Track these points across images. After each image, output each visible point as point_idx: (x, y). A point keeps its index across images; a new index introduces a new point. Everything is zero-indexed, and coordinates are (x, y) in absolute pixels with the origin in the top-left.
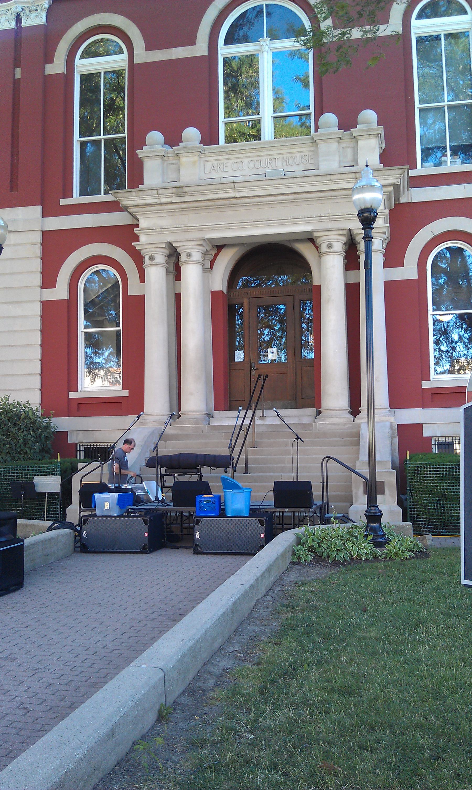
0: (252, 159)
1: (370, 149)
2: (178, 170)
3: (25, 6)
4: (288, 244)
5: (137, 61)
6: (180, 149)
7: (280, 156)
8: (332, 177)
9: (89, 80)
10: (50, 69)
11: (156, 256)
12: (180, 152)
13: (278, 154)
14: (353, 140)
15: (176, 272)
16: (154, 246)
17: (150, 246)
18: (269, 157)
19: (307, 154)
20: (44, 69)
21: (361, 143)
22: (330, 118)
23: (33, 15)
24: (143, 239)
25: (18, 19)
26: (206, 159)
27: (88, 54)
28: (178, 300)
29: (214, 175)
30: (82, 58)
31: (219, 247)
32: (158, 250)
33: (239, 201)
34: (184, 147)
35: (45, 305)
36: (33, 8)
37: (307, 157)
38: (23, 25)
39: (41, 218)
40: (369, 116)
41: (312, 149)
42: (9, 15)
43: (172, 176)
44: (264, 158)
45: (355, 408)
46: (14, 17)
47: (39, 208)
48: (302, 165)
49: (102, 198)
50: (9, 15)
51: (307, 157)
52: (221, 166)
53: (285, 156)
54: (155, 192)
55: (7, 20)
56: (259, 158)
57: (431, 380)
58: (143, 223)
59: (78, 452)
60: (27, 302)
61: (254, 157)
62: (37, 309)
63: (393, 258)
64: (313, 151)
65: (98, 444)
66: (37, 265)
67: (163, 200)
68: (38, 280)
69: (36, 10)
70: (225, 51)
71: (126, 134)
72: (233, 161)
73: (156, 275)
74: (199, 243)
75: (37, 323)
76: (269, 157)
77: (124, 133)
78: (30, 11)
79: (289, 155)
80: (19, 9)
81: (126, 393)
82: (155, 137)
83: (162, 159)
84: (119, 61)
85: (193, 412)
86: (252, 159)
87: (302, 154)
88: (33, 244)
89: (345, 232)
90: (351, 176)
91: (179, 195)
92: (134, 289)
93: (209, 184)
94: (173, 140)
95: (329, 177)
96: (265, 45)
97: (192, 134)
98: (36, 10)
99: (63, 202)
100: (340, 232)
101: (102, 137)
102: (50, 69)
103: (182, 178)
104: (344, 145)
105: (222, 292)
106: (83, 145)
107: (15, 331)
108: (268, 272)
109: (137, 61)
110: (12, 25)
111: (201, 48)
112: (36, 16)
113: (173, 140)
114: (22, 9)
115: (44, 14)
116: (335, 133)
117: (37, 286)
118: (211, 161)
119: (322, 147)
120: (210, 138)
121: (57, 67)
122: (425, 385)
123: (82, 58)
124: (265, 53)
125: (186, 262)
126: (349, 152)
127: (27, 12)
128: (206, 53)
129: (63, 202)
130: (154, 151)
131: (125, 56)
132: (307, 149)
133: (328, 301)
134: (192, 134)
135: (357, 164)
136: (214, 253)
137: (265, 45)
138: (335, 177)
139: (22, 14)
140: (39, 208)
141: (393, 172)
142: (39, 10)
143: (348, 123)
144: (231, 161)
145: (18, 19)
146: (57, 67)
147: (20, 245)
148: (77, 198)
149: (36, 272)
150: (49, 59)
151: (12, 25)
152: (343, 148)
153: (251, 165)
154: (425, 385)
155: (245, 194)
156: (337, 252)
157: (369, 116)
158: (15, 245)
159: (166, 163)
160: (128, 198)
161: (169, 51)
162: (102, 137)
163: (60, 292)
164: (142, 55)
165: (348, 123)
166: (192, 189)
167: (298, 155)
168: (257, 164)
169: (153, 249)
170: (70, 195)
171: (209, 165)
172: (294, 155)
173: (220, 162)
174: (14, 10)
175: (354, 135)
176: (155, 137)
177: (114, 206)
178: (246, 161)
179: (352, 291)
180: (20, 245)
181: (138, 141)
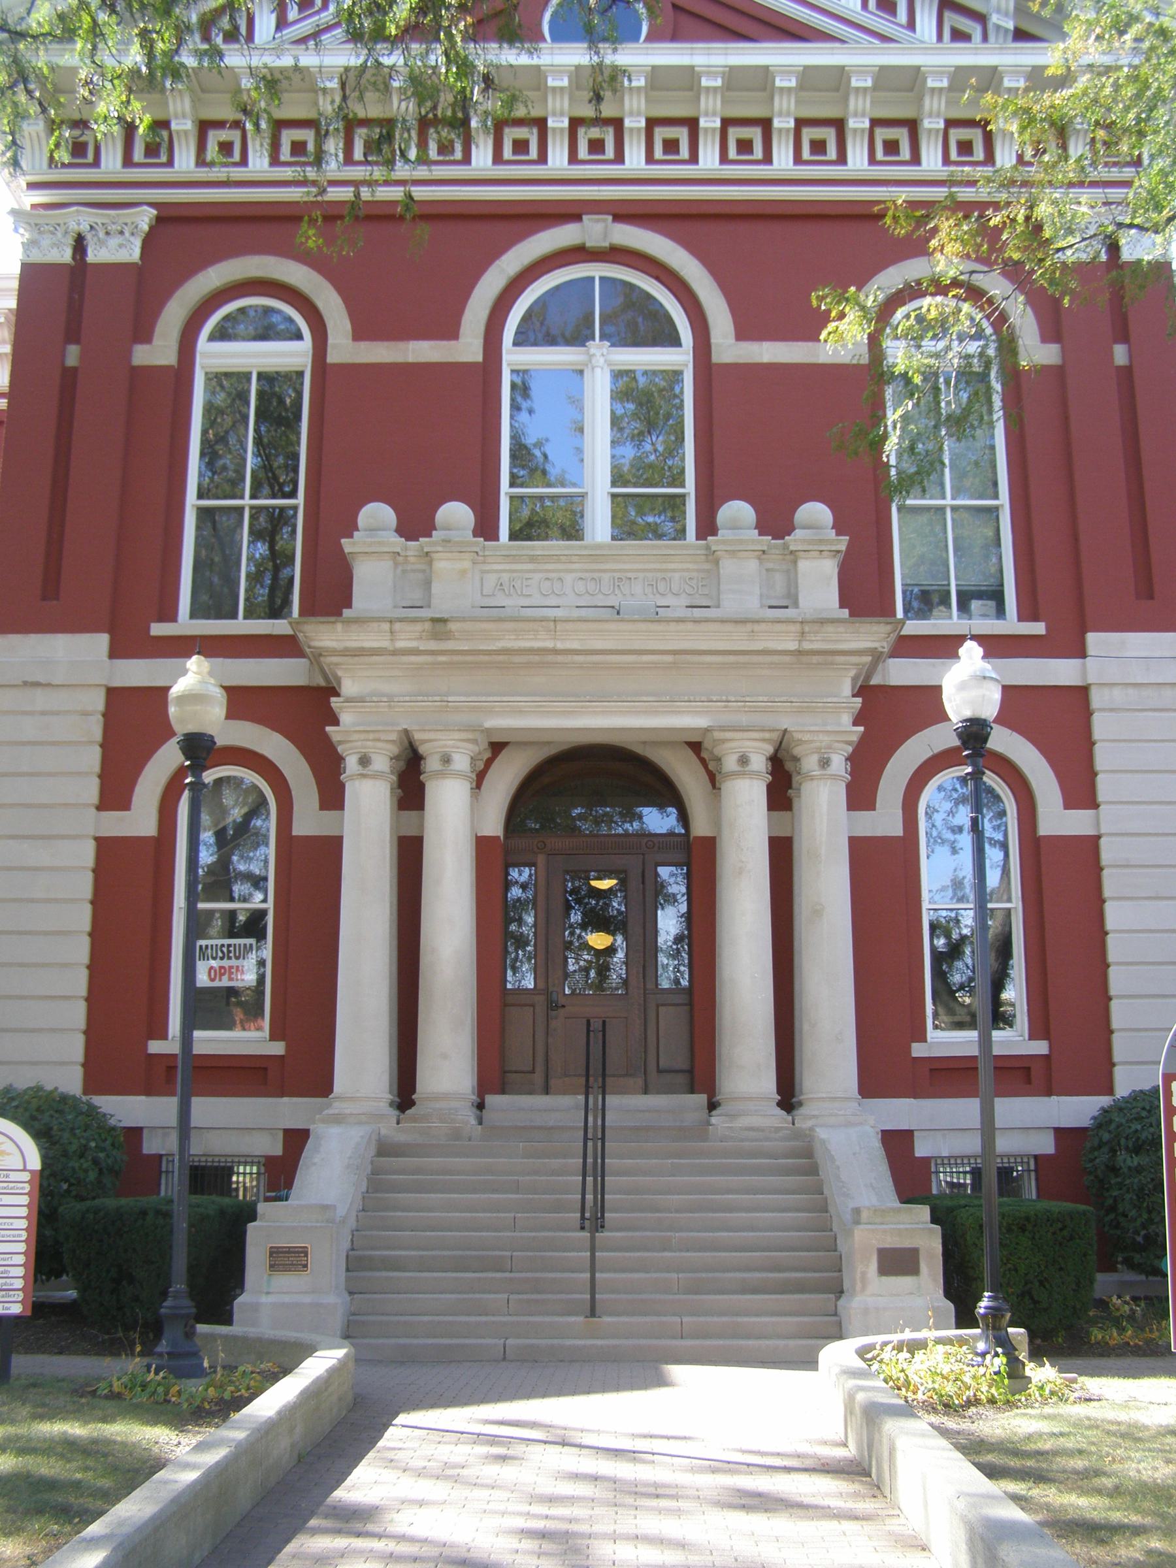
0: (583, 575)
1: (819, 584)
2: (427, 584)
3: (99, 222)
4: (639, 750)
5: (332, 357)
6: (435, 544)
7: (641, 575)
8: (756, 627)
9: (230, 383)
10: (142, 355)
11: (374, 757)
12: (433, 549)
13: (638, 571)
14: (788, 557)
15: (410, 788)
16: (371, 736)
17: (362, 736)
18: (617, 575)
19: (695, 574)
20: (129, 353)
21: (804, 565)
22: (737, 513)
23: (113, 242)
24: (346, 718)
25: (80, 245)
26: (487, 567)
27: (221, 334)
28: (410, 857)
29: (500, 600)
30: (212, 338)
31: (497, 748)
32: (380, 745)
33: (560, 658)
34: (443, 541)
35: (106, 847)
36: (113, 228)
37: (695, 581)
38: (91, 258)
39: (106, 659)
40: (815, 513)
41: (707, 566)
42: (59, 235)
43: (416, 596)
44: (606, 577)
45: (788, 1095)
46: (70, 241)
47: (102, 641)
48: (684, 595)
49: (241, 626)
50: (59, 235)
51: (695, 581)
52: (518, 585)
53: (650, 575)
54: (386, 626)
55: (57, 245)
56: (596, 575)
57: (929, 1039)
58: (349, 687)
59: (163, 1176)
60: (63, 837)
61: (586, 571)
62: (87, 854)
63: (861, 795)
64: (708, 571)
65: (210, 1159)
66: (92, 758)
67: (401, 644)
68: (91, 790)
69: (122, 233)
70: (513, 357)
71: (300, 500)
72: (541, 575)
73: (369, 802)
74: (470, 736)
75: (84, 886)
76: (617, 575)
77: (293, 494)
78: (107, 233)
79: (659, 575)
80: (84, 227)
81: (278, 1048)
82: (377, 515)
83: (394, 560)
84: (292, 355)
85: (445, 1097)
86: (583, 575)
87: (686, 574)
88: (85, 714)
89: (775, 736)
90: (792, 628)
91: (436, 636)
92: (309, 821)
93: (496, 616)
94: (415, 524)
95: (749, 627)
96: (598, 354)
97: (456, 514)
98: (122, 233)
99: (158, 629)
100: (767, 735)
101: (247, 501)
102: (142, 355)
103: (434, 602)
104: (770, 565)
105: (498, 837)
106: (205, 514)
107: (32, 901)
108: (589, 805)
109: (332, 357)
110: (65, 256)
111: (468, 348)
112: (121, 246)
113: (415, 524)
114: (91, 227)
115: (137, 244)
116: (753, 541)
117: (88, 805)
118: (496, 571)
119: (728, 566)
120: (486, 528)
121: (159, 351)
122: (918, 1050)
123: (212, 338)
124: (598, 371)
125: (441, 774)
126: (779, 579)
127: (101, 235)
128: (480, 359)
129: (158, 629)
130: (380, 543)
131: (306, 345)
132: (695, 567)
133: (740, 873)
134: (456, 514)
135: (796, 605)
136: (488, 755)
137: (598, 354)
138: (763, 626)
139: (89, 237)
140: (102, 641)
141: (875, 628)
142: (127, 234)
143: (775, 523)
144: (537, 577)
145: (80, 245)
146: (159, 351)
147: (57, 713)
148: (185, 624)
149: (87, 773)
150: (144, 333)
151: (65, 256)
152: (767, 570)
153: (580, 587)
154: (918, 1050)
155: (576, 645)
156: (834, 777)
157: (815, 513)
158: (43, 713)
159: (400, 568)
160: (325, 636)
161: (401, 345)
162: (247, 501)
163: (140, 820)
164: (344, 348)
165: (775, 523)
166: (467, 626)
167: (677, 575)
168: (591, 586)
169: (369, 743)
170: (172, 617)
171: (491, 580)
172: (669, 575)
173: (515, 575)
174: (73, 226)
175: (792, 548)
176: (377, 515)
177: (287, 646)
178: (569, 578)
179: (782, 855)
180: (57, 713)
181: (332, 521)
